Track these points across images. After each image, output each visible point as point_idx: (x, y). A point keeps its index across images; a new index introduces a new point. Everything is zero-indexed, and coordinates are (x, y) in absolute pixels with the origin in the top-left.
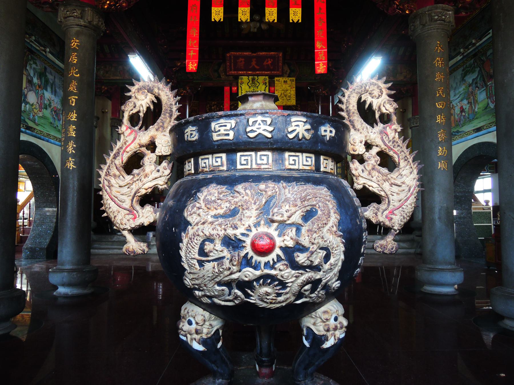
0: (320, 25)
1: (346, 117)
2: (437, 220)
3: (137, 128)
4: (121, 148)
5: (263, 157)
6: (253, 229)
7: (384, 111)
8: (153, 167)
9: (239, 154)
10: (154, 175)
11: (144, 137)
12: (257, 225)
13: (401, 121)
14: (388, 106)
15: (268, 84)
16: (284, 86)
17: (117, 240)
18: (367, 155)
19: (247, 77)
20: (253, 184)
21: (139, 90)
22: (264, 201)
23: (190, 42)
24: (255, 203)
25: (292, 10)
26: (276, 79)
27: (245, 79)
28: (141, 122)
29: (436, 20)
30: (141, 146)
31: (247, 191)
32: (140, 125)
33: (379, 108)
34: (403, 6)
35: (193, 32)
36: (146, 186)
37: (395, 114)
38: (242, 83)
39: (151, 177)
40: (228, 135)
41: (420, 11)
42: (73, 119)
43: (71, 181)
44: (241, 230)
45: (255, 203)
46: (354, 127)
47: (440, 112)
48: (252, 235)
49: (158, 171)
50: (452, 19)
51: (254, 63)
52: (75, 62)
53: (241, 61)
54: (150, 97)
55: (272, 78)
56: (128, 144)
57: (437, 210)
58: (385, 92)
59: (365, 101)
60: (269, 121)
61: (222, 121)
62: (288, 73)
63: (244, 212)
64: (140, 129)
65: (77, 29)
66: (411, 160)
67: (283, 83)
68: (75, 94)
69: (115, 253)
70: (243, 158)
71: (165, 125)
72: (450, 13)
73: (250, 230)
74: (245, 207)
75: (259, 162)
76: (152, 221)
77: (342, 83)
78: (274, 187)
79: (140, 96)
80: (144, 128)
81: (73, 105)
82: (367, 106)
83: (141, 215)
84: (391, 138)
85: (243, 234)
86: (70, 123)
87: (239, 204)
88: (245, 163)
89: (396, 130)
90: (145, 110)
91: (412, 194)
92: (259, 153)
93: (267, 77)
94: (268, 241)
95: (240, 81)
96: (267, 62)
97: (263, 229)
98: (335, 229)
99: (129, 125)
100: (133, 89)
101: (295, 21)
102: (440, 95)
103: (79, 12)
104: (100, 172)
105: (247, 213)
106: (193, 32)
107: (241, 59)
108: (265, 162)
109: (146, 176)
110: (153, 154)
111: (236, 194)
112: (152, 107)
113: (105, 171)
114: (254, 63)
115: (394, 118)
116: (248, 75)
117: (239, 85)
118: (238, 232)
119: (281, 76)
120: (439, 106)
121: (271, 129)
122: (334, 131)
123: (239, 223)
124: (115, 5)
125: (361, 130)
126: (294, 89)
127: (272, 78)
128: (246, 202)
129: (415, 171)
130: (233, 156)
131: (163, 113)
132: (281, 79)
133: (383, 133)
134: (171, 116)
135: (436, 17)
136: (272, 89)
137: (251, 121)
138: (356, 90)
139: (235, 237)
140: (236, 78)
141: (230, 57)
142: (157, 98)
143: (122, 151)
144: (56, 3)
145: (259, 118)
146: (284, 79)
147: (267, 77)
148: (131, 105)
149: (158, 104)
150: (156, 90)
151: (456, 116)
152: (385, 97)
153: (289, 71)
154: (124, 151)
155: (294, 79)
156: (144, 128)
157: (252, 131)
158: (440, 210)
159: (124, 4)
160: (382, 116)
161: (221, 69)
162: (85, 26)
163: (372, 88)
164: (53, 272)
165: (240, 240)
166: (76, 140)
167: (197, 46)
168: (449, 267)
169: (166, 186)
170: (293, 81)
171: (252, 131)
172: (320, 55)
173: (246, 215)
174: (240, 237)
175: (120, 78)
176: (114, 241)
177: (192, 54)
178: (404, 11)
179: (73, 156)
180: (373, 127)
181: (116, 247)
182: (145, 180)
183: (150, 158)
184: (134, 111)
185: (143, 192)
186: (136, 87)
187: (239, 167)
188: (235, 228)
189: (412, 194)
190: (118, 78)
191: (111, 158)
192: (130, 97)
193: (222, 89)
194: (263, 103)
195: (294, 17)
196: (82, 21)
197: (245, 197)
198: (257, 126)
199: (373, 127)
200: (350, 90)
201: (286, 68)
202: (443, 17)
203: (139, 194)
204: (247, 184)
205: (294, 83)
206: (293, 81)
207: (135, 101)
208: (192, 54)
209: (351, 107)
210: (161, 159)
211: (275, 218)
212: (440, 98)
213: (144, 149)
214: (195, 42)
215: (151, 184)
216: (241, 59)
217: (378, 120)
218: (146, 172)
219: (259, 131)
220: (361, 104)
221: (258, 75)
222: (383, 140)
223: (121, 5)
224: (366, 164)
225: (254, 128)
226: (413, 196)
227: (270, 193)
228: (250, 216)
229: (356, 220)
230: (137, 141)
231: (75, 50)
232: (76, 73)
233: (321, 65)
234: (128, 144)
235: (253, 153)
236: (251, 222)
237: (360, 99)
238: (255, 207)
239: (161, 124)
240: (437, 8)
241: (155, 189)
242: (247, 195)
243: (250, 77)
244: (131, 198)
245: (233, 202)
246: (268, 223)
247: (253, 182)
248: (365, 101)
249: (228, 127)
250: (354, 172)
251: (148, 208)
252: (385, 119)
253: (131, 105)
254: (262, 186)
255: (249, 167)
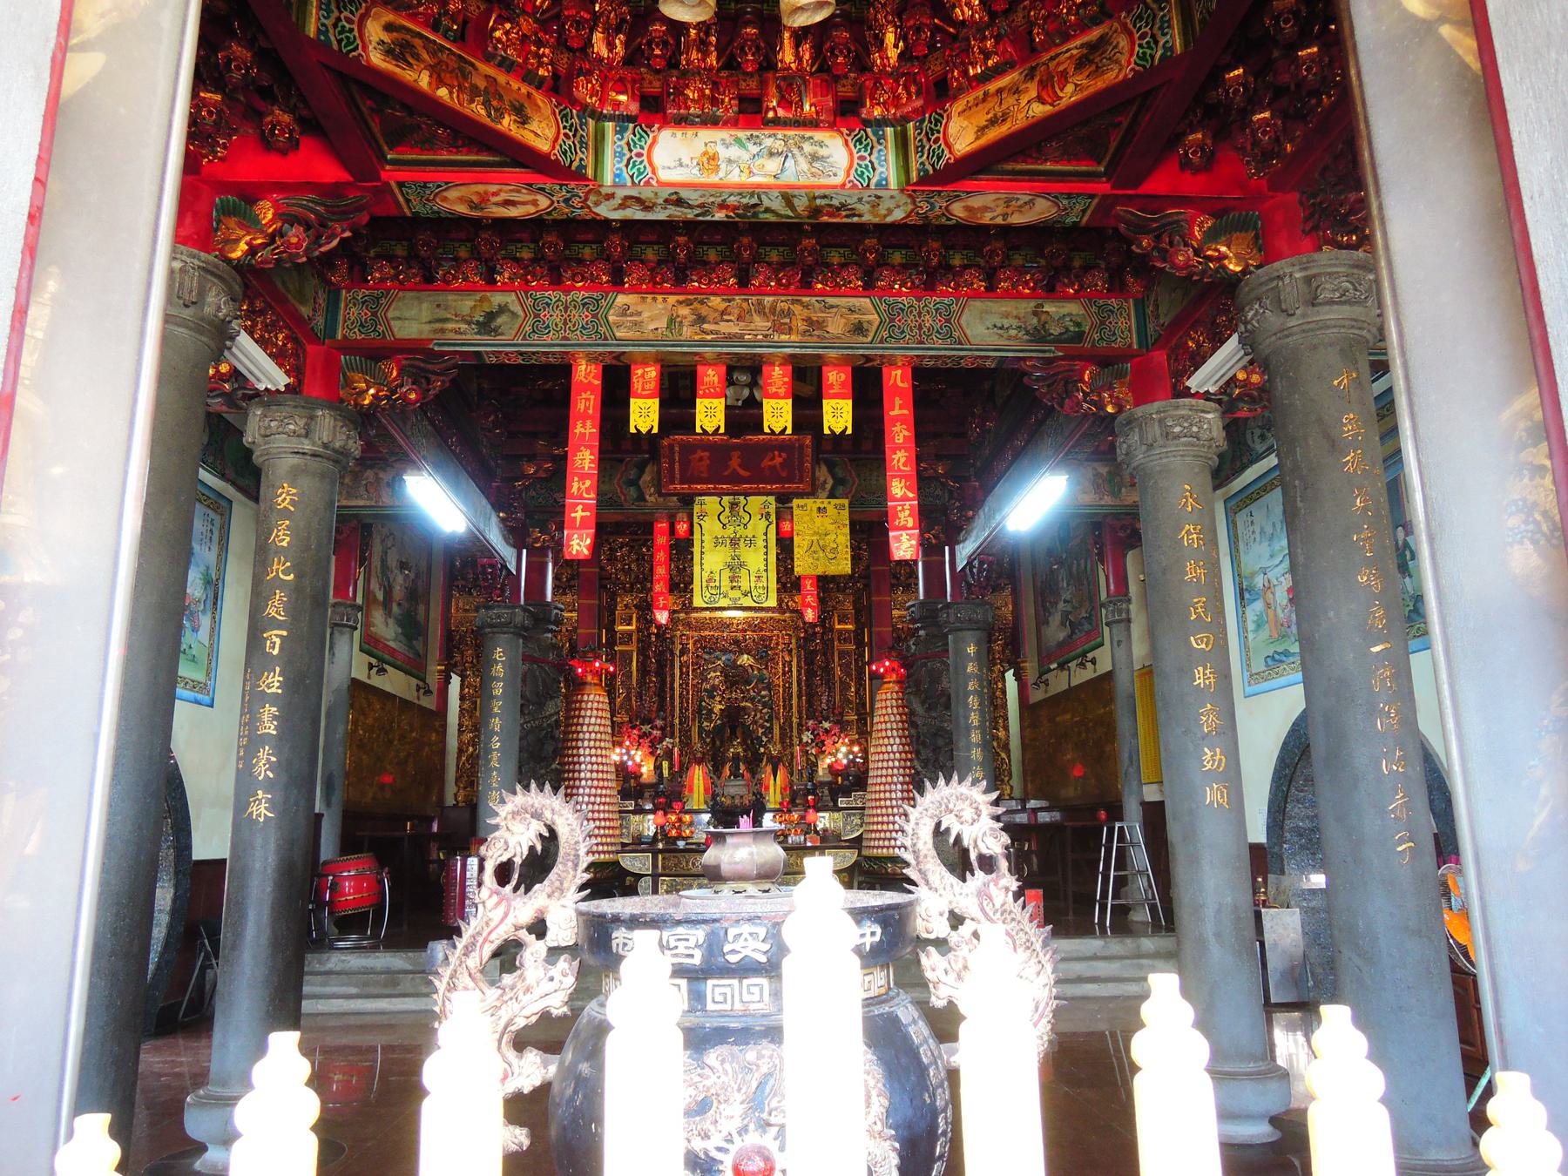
0: (899, 440)
1: (913, 862)
2: (1212, 939)
3: (509, 888)
4: (479, 933)
5: (753, 989)
6: (736, 1138)
7: (985, 851)
8: (541, 972)
9: (710, 983)
10: (545, 986)
11: (524, 908)
12: (743, 1131)
13: (1016, 869)
14: (990, 841)
15: (773, 518)
16: (818, 521)
17: (338, 969)
18: (954, 938)
19: (717, 499)
20: (735, 1048)
21: (515, 814)
22: (754, 1084)
23: (575, 486)
24: (739, 1090)
25: (828, 405)
26: (796, 502)
27: (711, 503)
28: (516, 876)
29: (1177, 437)
30: (517, 928)
31: (727, 1066)
32: (514, 882)
33: (976, 846)
34: (1099, 395)
35: (585, 459)
36: (527, 1012)
37: (1008, 857)
38: (703, 515)
39: (537, 992)
40: (692, 956)
41: (1140, 411)
42: (274, 690)
43: (259, 853)
44: (717, 1140)
45: (739, 1090)
46: (927, 883)
47: (1203, 658)
48: (734, 1149)
49: (552, 979)
50: (1218, 433)
51: (735, 463)
52: (284, 544)
53: (701, 459)
54: (537, 827)
55: (784, 499)
56: (492, 925)
57: (1209, 913)
58: (987, 810)
59: (948, 830)
60: (762, 932)
61: (680, 930)
62: (828, 487)
63: (722, 1107)
64: (516, 889)
65: (295, 460)
66: (1038, 946)
67: (815, 513)
68: (280, 626)
69: (335, 1010)
70: (718, 990)
71: (566, 885)
72: (1210, 416)
73: (731, 1141)
74: (722, 1098)
75: (746, 998)
76: (538, 1083)
77: (973, 517)
78: (771, 1057)
79: (517, 827)
80: (522, 889)
81: (275, 652)
82: (952, 840)
83: (516, 1071)
84: (998, 905)
85: (719, 1149)
86: (264, 698)
87: (713, 1091)
88: (721, 999)
89: (1007, 889)
90: (526, 852)
91: (1041, 1017)
92: (746, 982)
93: (772, 499)
94: (762, 1165)
95: (697, 509)
96: (772, 459)
97: (753, 1138)
98: (879, 1127)
99: (495, 886)
100: (503, 811)
101: (838, 431)
102: (1199, 617)
103: (302, 422)
104: (437, 983)
105: (727, 1110)
106: (585, 459)
107: (700, 453)
108: (756, 997)
109: (527, 990)
110: (541, 942)
111: (707, 1071)
112: (539, 848)
113: (445, 980)
114: (735, 463)
115: (1004, 864)
116: (720, 495)
117: (696, 520)
118: (710, 1145)
119: (812, 494)
120: (1198, 643)
121: (766, 947)
122: (879, 930)
123: (712, 1128)
124: (388, 397)
125: (941, 891)
126: (847, 530)
127: (784, 499)
128: (724, 1088)
129: (1049, 968)
130: (701, 986)
131: (560, 859)
132: (809, 502)
133: (983, 894)
134: (576, 865)
135: (1177, 429)
136: (786, 526)
137: (732, 932)
138: (931, 811)
139: (706, 1154)
140: (687, 501)
141: (671, 447)
142: (552, 831)
143: (481, 940)
144: (240, 393)
145: (746, 928)
146: (819, 503)
147: (772, 499)
148: (500, 845)
149: (551, 838)
150: (548, 814)
151: (1279, 611)
152: (986, 823)
153: (830, 482)
154: (485, 940)
155: (846, 502)
156: (522, 889)
157: (733, 952)
158: (1219, 911)
159: (413, 396)
160: (981, 857)
161: (647, 477)
162: (314, 455)
163: (960, 805)
164: (200, 1105)
165: (713, 1160)
166: (280, 741)
167: (593, 495)
168: (1251, 1067)
169: (565, 1009)
170: (842, 507)
171: (733, 952)
172: (901, 515)
173: (724, 1114)
174: (714, 1154)
175: (368, 503)
176: (329, 973)
177: (579, 514)
178: (1100, 405)
179: (269, 785)
180: (964, 880)
181: (336, 989)
182: (525, 999)
183: (535, 950)
184: (504, 858)
185: (521, 1022)
186: (509, 807)
187: (710, 1006)
188: (706, 1136)
189: (1041, 1017)
190: (361, 503)
191: (459, 951)
192: (496, 827)
193: (648, 528)
194: (754, 849)
195: (833, 421)
196: (306, 441)
197: (724, 1078)
198: (741, 942)
199: (964, 880)
200: (919, 809)
201: (823, 473)
202: (1195, 429)
203: (513, 1028)
204: (723, 1050)
205: (846, 513)
206: (842, 507)
207: (507, 835)
208: (579, 514)
209: (920, 846)
210: (554, 952)
211: (773, 1120)
212: (1200, 625)
213: (523, 935)
214: (588, 483)
215: (538, 1007)
216: (700, 453)
217: (975, 864)
218: (528, 982)
219: (745, 952)
220: (939, 833)
221: (746, 494)
222: (983, 910)
223: (404, 397)
224: (950, 955)
225: (736, 946)
226: (1044, 1021)
227: (764, 1070)
228: (731, 1114)
229: (922, 1095)
230: (510, 920)
231: (285, 514)
232: (286, 573)
233: (904, 537)
234: (492, 925)
235: (735, 982)
236: (732, 1126)
237: (938, 824)
238: (739, 1097)
239: (557, 884)
240: (1177, 407)
241: (545, 1016)
242: (726, 1073)
243: (726, 499)
244: (497, 1036)
245: (700, 1086)
246: (761, 1127)
247: (735, 1043)
248: (948, 830)
249: (692, 943)
250: (929, 974)
251: (532, 1056)
252: (988, 864)
253: (500, 845)
254: (751, 1055)
255: (727, 1007)
